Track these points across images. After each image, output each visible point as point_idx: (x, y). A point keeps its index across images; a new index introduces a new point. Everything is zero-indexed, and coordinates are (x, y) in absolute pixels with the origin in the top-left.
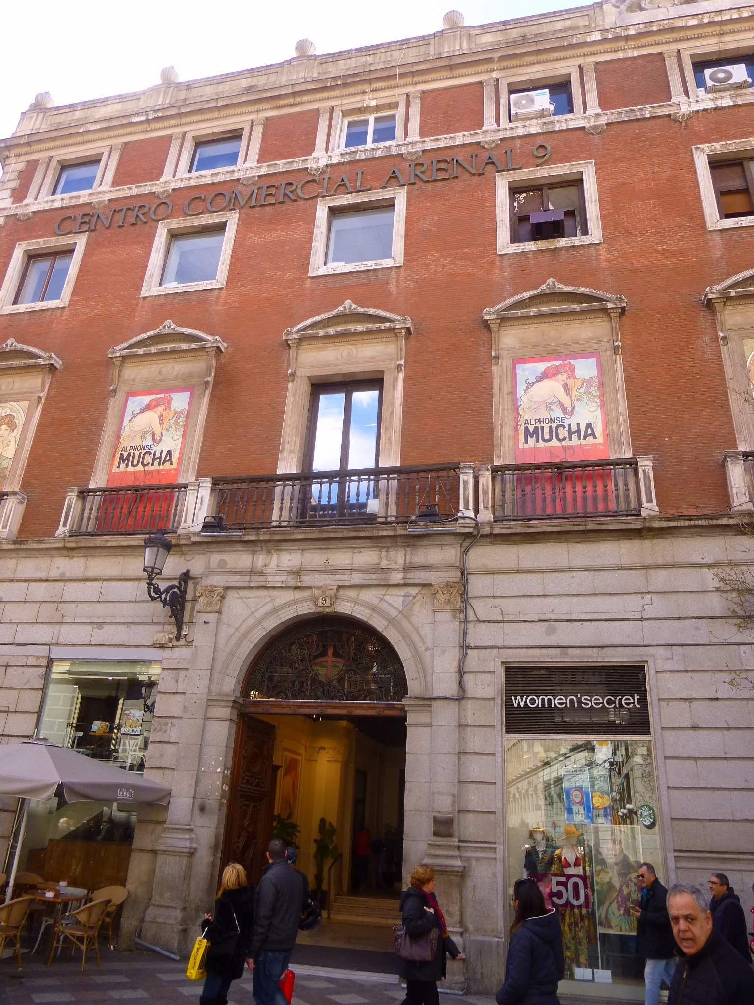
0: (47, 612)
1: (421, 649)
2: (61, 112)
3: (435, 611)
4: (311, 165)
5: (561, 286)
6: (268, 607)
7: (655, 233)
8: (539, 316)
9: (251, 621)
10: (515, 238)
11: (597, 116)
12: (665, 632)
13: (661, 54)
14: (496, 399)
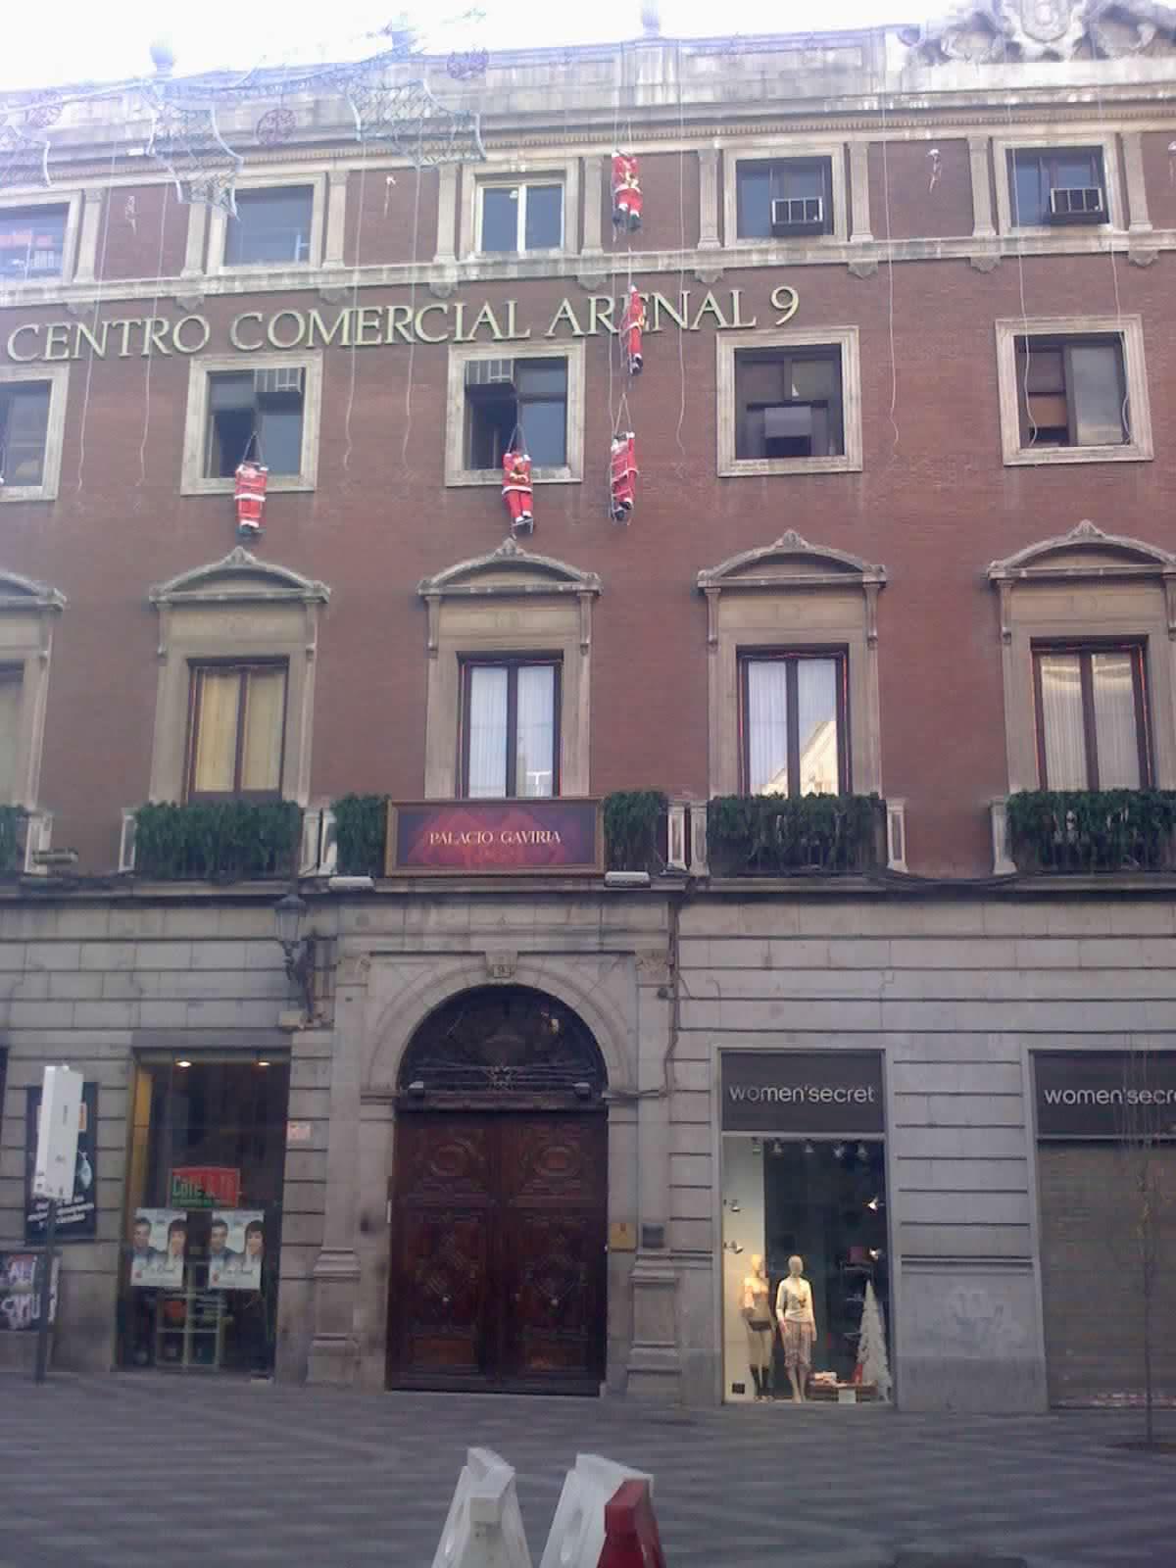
0: (117, 985)
3: (638, 986)
4: (431, 278)
5: (804, 542)
6: (429, 978)
10: (742, 452)
11: (867, 246)
12: (906, 1016)
13: (964, 140)
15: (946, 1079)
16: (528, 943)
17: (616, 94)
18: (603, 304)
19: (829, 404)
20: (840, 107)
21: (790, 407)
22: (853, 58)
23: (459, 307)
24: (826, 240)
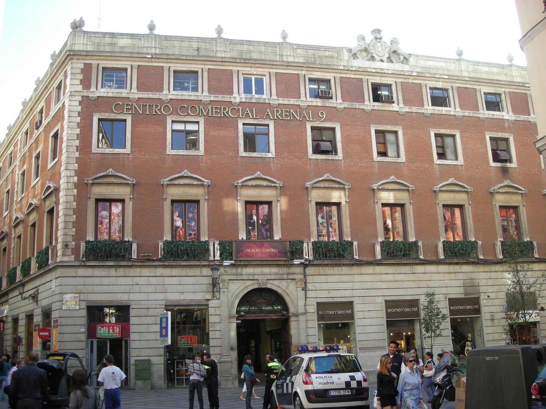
0: (159, 288)
1: (293, 299)
2: (97, 36)
6: (244, 286)
7: (358, 159)
8: (324, 188)
9: (238, 291)
11: (341, 103)
12: (358, 293)
14: (310, 216)
15: (366, 307)
16: (269, 277)
17: (278, 56)
18: (277, 111)
19: (333, 142)
20: (334, 68)
21: (323, 143)
22: (335, 55)
23: (240, 108)
24: (330, 101)
